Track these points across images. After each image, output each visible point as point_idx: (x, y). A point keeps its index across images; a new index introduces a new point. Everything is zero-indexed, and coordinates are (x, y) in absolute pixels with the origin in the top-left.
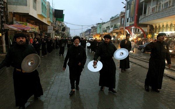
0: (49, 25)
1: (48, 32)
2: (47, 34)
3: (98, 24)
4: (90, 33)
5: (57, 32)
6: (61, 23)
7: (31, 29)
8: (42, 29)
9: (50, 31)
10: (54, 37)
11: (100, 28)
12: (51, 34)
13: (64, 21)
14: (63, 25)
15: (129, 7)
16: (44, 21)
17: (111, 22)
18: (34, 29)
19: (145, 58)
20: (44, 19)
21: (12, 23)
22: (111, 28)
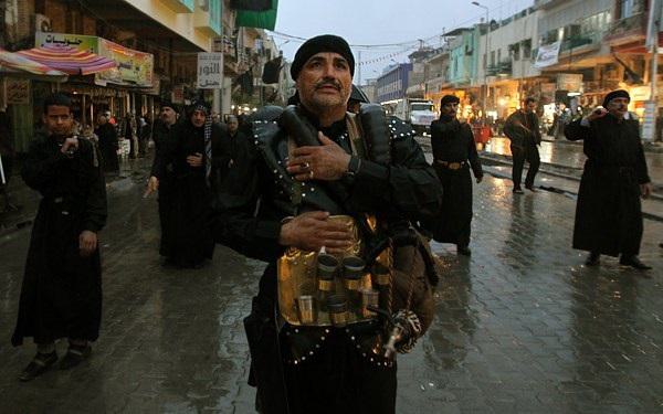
0: (205, 49)
1: (202, 81)
2: (189, 94)
3: (458, 32)
4: (405, 85)
5: (243, 83)
6: (259, 37)
7: (114, 70)
8: (171, 70)
9: (212, 78)
10: (226, 111)
11: (470, 54)
12: (210, 92)
13: (276, 28)
14: (269, 51)
15: (140, 145)
16: (182, 27)
17: (538, 14)
18: (129, 67)
19: (24, 146)
20: (180, 16)
21: (27, 43)
22: (541, 50)
